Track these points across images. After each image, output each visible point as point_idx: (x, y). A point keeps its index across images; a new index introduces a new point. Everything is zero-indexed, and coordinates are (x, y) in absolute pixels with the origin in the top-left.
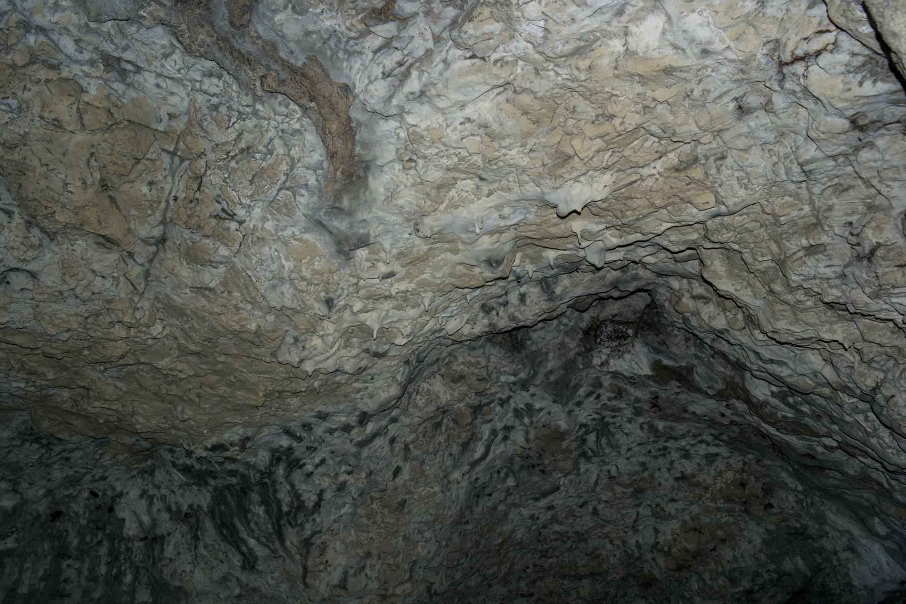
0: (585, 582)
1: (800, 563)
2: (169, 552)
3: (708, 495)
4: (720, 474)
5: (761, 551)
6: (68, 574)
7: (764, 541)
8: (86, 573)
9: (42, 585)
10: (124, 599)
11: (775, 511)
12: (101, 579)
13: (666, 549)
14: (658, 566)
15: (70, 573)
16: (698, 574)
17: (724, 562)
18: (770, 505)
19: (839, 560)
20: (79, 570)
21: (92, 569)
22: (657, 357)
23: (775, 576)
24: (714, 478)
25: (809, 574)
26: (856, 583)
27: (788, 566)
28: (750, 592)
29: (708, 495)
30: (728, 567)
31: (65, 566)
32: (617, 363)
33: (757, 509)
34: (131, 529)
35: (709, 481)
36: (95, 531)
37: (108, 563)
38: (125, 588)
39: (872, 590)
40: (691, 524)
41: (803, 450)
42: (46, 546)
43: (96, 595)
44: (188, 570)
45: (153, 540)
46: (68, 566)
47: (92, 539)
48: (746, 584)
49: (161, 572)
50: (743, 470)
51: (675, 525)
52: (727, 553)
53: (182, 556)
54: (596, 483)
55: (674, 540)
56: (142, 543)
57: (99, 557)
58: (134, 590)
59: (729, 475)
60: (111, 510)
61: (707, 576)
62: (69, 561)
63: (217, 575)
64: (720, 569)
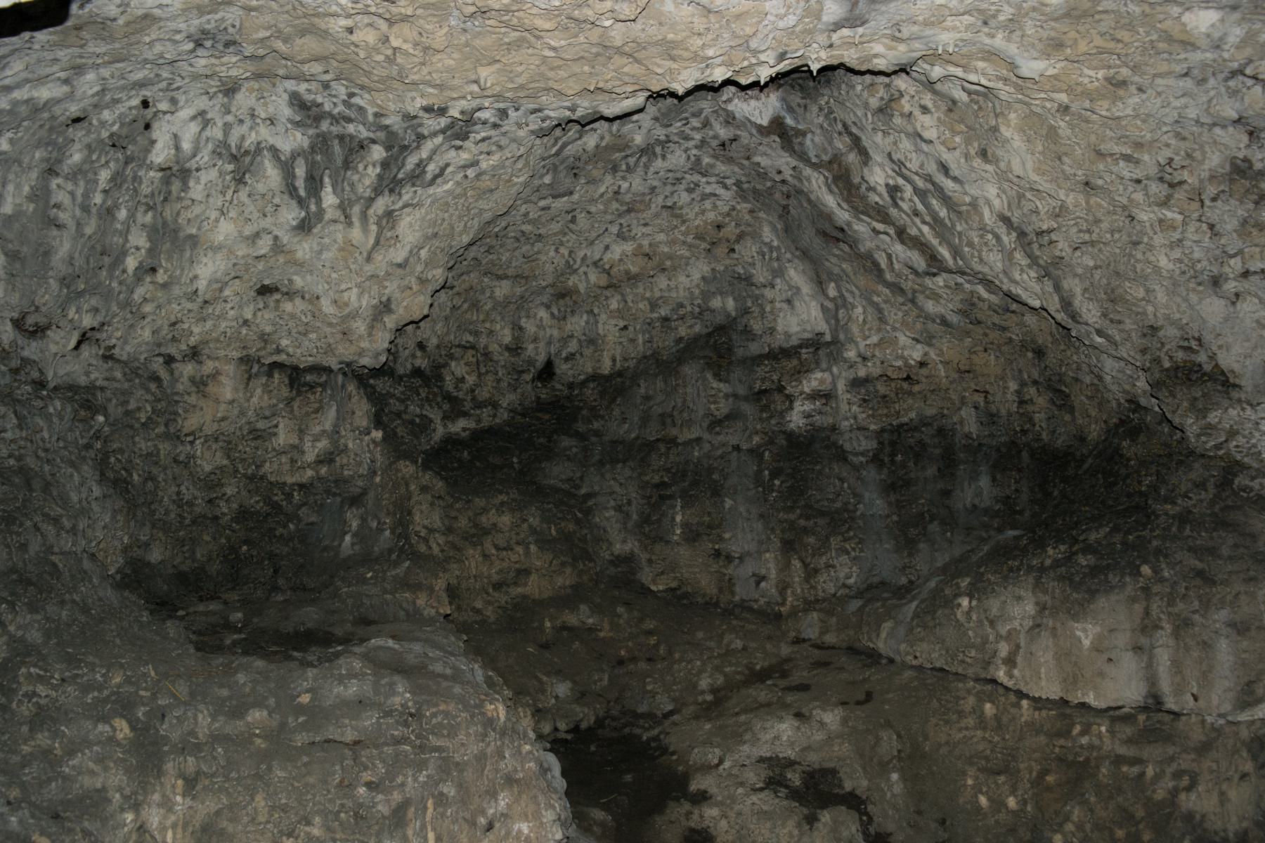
0: (505, 283)
1: (731, 304)
2: (196, 191)
3: (683, 228)
4: (703, 212)
5: (698, 286)
6: (60, 198)
7: (703, 278)
8: (79, 199)
9: (32, 207)
10: (115, 239)
11: (736, 256)
12: (94, 210)
13: (607, 267)
14: (588, 281)
15: (61, 197)
16: (623, 295)
17: (656, 290)
18: (733, 250)
19: (773, 309)
20: (72, 194)
21: (86, 195)
22: (783, 113)
23: (697, 310)
24: (697, 214)
25: (733, 314)
26: (779, 328)
27: (716, 303)
28: (666, 319)
29: (683, 228)
30: (658, 294)
31: (55, 187)
32: (740, 104)
33: (721, 250)
34: (161, 154)
35: (691, 215)
36: (108, 148)
37: (105, 191)
38: (119, 226)
39: (790, 336)
40: (646, 249)
41: (840, 223)
42: (37, 155)
43: (89, 231)
44: (213, 218)
45: (178, 172)
46: (59, 186)
47: (99, 158)
48: (664, 312)
49: (178, 214)
50: (728, 215)
51: (629, 247)
52: (662, 282)
53: (211, 200)
54: (602, 195)
55: (621, 260)
56: (160, 174)
57: (96, 182)
58: (128, 231)
59: (711, 216)
60: (147, 126)
61: (629, 298)
62: (59, 181)
63: (248, 230)
64: (648, 295)
